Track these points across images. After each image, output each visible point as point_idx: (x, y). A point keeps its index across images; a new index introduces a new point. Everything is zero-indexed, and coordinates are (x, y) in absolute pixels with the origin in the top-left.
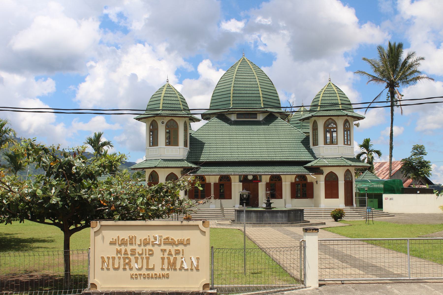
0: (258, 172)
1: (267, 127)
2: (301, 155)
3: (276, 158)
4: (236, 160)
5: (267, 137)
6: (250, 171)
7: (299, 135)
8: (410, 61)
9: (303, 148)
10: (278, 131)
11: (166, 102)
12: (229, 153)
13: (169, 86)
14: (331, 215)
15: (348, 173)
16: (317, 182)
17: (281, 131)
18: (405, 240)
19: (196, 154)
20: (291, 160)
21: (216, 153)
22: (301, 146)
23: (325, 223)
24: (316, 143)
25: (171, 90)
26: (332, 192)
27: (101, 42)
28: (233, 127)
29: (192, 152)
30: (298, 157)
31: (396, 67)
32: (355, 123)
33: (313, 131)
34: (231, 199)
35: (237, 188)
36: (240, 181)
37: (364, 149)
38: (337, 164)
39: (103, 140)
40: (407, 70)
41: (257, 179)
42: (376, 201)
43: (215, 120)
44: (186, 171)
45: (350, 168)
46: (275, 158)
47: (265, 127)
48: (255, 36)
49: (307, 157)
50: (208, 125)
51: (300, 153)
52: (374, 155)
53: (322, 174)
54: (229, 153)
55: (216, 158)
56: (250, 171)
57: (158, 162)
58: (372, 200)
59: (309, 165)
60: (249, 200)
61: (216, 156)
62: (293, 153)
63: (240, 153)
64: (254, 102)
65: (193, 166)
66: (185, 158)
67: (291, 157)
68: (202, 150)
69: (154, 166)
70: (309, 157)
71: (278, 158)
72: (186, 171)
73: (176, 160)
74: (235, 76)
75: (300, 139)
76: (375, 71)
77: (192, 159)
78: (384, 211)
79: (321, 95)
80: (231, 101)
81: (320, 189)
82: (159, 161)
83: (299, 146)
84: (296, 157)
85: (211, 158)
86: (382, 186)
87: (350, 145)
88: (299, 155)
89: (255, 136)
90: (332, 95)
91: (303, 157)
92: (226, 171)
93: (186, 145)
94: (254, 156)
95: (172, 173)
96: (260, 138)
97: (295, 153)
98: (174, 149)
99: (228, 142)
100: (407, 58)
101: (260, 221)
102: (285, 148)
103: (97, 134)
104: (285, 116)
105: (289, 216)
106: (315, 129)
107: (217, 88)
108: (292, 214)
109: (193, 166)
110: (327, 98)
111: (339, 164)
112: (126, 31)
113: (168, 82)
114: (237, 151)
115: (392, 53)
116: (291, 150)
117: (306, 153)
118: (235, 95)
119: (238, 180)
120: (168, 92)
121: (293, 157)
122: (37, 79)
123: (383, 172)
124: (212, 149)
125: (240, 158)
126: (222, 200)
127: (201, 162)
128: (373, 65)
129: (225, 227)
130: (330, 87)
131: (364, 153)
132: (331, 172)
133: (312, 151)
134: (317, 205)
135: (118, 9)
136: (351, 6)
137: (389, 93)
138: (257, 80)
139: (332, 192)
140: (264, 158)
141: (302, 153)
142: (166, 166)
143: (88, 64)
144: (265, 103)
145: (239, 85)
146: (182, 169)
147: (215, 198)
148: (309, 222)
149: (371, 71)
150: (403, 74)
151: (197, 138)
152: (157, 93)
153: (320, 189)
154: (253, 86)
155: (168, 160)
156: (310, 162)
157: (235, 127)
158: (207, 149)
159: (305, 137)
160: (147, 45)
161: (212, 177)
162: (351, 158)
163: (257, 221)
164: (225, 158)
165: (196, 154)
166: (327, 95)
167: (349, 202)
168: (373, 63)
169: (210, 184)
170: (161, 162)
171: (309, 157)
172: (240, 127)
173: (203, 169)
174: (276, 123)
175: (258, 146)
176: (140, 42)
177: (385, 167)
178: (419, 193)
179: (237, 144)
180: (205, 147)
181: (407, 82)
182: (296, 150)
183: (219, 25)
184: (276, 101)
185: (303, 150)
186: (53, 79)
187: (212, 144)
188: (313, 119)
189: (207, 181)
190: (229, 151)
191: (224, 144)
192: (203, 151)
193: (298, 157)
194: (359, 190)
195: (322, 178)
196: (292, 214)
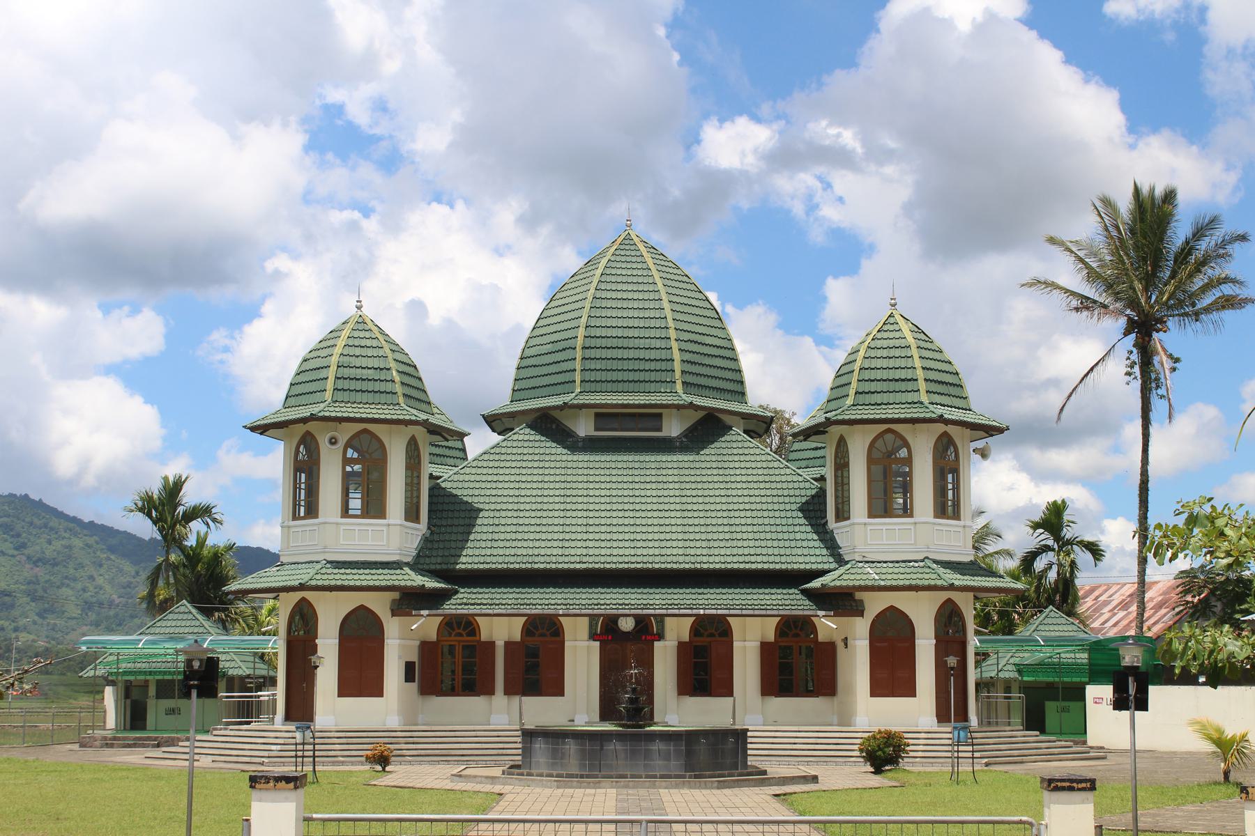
0: (646, 607)
1: (691, 458)
2: (795, 551)
4: (578, 566)
5: (689, 493)
6: (626, 603)
7: (796, 485)
8: (1204, 245)
9: (803, 528)
12: (555, 544)
13: (361, 321)
14: (861, 750)
15: (949, 618)
16: (845, 640)
17: (738, 472)
18: (632, 822)
19: (447, 545)
20: (760, 566)
21: (514, 544)
22: (797, 521)
23: (815, 779)
24: (843, 514)
25: (367, 335)
26: (892, 676)
27: (308, 198)
28: (581, 457)
29: (436, 537)
30: (783, 559)
31: (1156, 266)
33: (836, 470)
34: (563, 695)
35: (582, 661)
36: (593, 636)
38: (907, 583)
39: (190, 497)
40: (1191, 276)
41: (647, 630)
43: (523, 434)
44: (409, 601)
45: (956, 597)
46: (705, 559)
47: (686, 458)
48: (806, 179)
49: (813, 559)
50: (498, 450)
51: (793, 544)
52: (1083, 557)
53: (861, 613)
54: (555, 544)
55: (512, 559)
56: (626, 603)
57: (312, 572)
58: (1046, 703)
59: (816, 584)
60: (626, 700)
61: (513, 552)
62: (769, 544)
63: (591, 544)
64: (653, 376)
65: (431, 584)
66: (409, 559)
67: (759, 559)
68: (470, 533)
69: (297, 583)
70: (819, 559)
71: (717, 559)
72: (409, 601)
73: (376, 563)
74: (592, 291)
75: (798, 499)
77: (433, 560)
79: (862, 353)
80: (578, 373)
81: (857, 666)
82: (319, 566)
83: (790, 521)
84: (777, 559)
85: (494, 559)
86: (1083, 657)
88: (788, 551)
89: (648, 486)
90: (897, 353)
91: (801, 559)
93: (412, 514)
94: (639, 552)
95: (362, 607)
97: (775, 544)
99: (557, 507)
100: (1194, 235)
101: (592, 767)
102: (744, 529)
103: (171, 479)
104: (760, 425)
105: (689, 754)
106: (842, 466)
107: (538, 332)
108: (702, 747)
109: (431, 584)
110: (879, 363)
111: (914, 583)
112: (392, 161)
113: (359, 308)
114: (585, 536)
115: (1142, 220)
116: (762, 536)
117: (811, 544)
118: (592, 353)
120: (357, 342)
121: (765, 559)
122: (106, 309)
124: (502, 529)
125: (591, 559)
126: (524, 698)
127: (461, 570)
128: (1081, 260)
129: (478, 787)
130: (891, 327)
131: (1047, 548)
132: (892, 607)
133: (833, 539)
134: (845, 719)
135: (368, 90)
136: (1109, 81)
137: (1135, 351)
138: (666, 305)
139: (892, 676)
140: (669, 559)
141: (799, 544)
142: (339, 583)
143: (270, 266)
144: (690, 379)
145: (604, 322)
147: (509, 692)
148: (765, 773)
150: (1177, 288)
151: (458, 492)
152: (322, 345)
153: (857, 666)
154: (653, 323)
155: (350, 563)
156: (822, 573)
157: (586, 458)
158: (485, 529)
159: (814, 492)
160: (460, 205)
161: (500, 620)
162: (959, 563)
163: (582, 766)
165: (447, 545)
166: (879, 353)
167: (950, 707)
168: (1081, 254)
169: (491, 645)
170: (324, 571)
171: (819, 559)
172: (603, 458)
173: (464, 594)
174: (724, 445)
175: (656, 522)
176: (438, 198)
178: (1204, 684)
180: (479, 521)
181: (1197, 315)
182: (780, 536)
183: (692, 140)
184: (729, 375)
185: (804, 536)
186: (160, 310)
187: (503, 514)
188: (835, 430)
189: (484, 636)
190: (556, 536)
192: (472, 537)
193: (783, 559)
194: (1019, 671)
195: (859, 632)
196: (702, 747)
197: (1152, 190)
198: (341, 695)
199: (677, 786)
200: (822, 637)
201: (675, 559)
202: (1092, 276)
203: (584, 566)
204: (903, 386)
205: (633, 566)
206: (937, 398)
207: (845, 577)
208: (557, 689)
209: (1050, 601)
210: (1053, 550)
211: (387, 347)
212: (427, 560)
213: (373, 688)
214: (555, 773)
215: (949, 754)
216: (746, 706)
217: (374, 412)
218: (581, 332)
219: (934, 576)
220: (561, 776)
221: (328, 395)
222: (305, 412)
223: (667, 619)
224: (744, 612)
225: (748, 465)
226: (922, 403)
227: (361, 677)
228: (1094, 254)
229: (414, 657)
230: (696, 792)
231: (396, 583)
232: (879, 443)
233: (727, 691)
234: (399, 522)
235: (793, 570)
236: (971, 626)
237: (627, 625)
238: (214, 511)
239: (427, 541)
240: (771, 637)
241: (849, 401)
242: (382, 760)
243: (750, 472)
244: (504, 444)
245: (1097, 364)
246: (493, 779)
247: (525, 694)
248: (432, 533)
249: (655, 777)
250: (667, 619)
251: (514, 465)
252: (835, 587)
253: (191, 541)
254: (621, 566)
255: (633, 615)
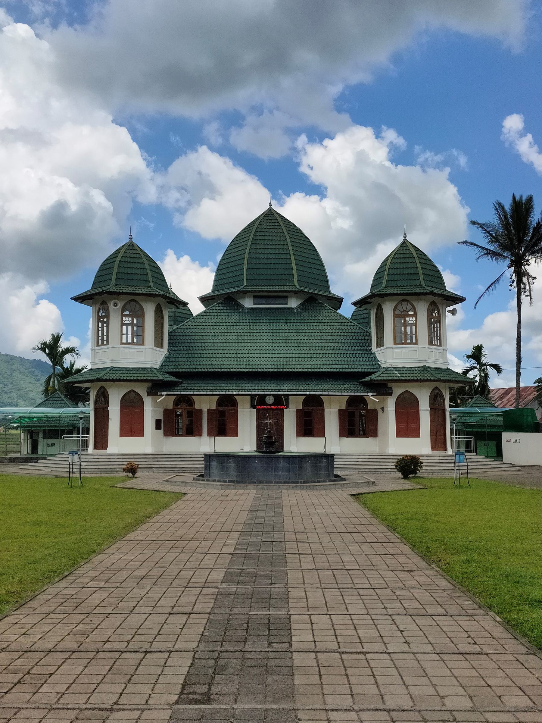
3: (313, 367)
4: (244, 370)
6: (270, 390)
10: (320, 324)
11: (123, 270)
14: (396, 466)
16: (382, 409)
24: (380, 343)
25: (134, 252)
26: (407, 427)
29: (172, 356)
32: (448, 309)
36: (253, 407)
37: (475, 362)
39: (63, 345)
41: (281, 402)
42: (493, 444)
44: (156, 387)
52: (492, 372)
53: (391, 394)
56: (270, 390)
59: (368, 379)
60: (270, 440)
69: (96, 378)
71: (316, 367)
76: (491, 241)
77: (170, 367)
78: (505, 461)
81: (389, 419)
87: (440, 345)
90: (408, 260)
92: (229, 389)
93: (159, 343)
96: (289, 334)
98: (136, 350)
111: (419, 378)
119: (249, 405)
123: (509, 402)
125: (251, 367)
128: (488, 232)
130: (405, 248)
131: (473, 368)
137: (514, 275)
140: (291, 367)
142: (118, 378)
146: (150, 384)
147: (210, 434)
149: (484, 242)
153: (389, 419)
161: (205, 401)
164: (226, 367)
166: (399, 261)
167: (438, 442)
177: (513, 395)
179: (248, 345)
189: (197, 407)
191: (228, 345)
195: (391, 405)
197: (521, 198)
198: (121, 435)
199: (293, 488)
200: (370, 407)
201: (294, 367)
202: (494, 240)
203: (247, 370)
204: (411, 277)
205: (272, 370)
206: (429, 283)
207: (382, 375)
208: (235, 433)
209: (476, 392)
210: (477, 368)
211: (146, 262)
212: (167, 367)
213: (139, 433)
214: (222, 479)
215: (453, 468)
216: (331, 442)
217: (137, 290)
218: (247, 256)
219: (429, 375)
220: (224, 481)
221: (113, 281)
222: (100, 290)
223: (290, 397)
224: (330, 393)
225: (331, 321)
226: (421, 285)
227: (132, 427)
228: (495, 229)
229: (161, 417)
230: (304, 492)
231: (149, 378)
232: (399, 307)
233: (321, 434)
234: (151, 347)
235: (355, 372)
236: (447, 403)
237: (270, 400)
238: (76, 350)
239: (167, 358)
240: (344, 408)
241: (384, 285)
242: (132, 470)
243: (332, 324)
244: (208, 311)
245: (495, 281)
246: (185, 483)
247: (217, 436)
248: (170, 354)
249: (280, 482)
250: (290, 397)
251: (213, 321)
252: (377, 380)
253: (67, 365)
254: (266, 370)
255: (273, 395)
